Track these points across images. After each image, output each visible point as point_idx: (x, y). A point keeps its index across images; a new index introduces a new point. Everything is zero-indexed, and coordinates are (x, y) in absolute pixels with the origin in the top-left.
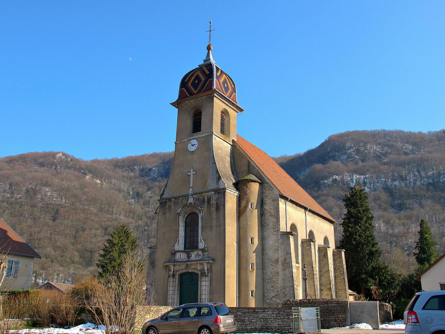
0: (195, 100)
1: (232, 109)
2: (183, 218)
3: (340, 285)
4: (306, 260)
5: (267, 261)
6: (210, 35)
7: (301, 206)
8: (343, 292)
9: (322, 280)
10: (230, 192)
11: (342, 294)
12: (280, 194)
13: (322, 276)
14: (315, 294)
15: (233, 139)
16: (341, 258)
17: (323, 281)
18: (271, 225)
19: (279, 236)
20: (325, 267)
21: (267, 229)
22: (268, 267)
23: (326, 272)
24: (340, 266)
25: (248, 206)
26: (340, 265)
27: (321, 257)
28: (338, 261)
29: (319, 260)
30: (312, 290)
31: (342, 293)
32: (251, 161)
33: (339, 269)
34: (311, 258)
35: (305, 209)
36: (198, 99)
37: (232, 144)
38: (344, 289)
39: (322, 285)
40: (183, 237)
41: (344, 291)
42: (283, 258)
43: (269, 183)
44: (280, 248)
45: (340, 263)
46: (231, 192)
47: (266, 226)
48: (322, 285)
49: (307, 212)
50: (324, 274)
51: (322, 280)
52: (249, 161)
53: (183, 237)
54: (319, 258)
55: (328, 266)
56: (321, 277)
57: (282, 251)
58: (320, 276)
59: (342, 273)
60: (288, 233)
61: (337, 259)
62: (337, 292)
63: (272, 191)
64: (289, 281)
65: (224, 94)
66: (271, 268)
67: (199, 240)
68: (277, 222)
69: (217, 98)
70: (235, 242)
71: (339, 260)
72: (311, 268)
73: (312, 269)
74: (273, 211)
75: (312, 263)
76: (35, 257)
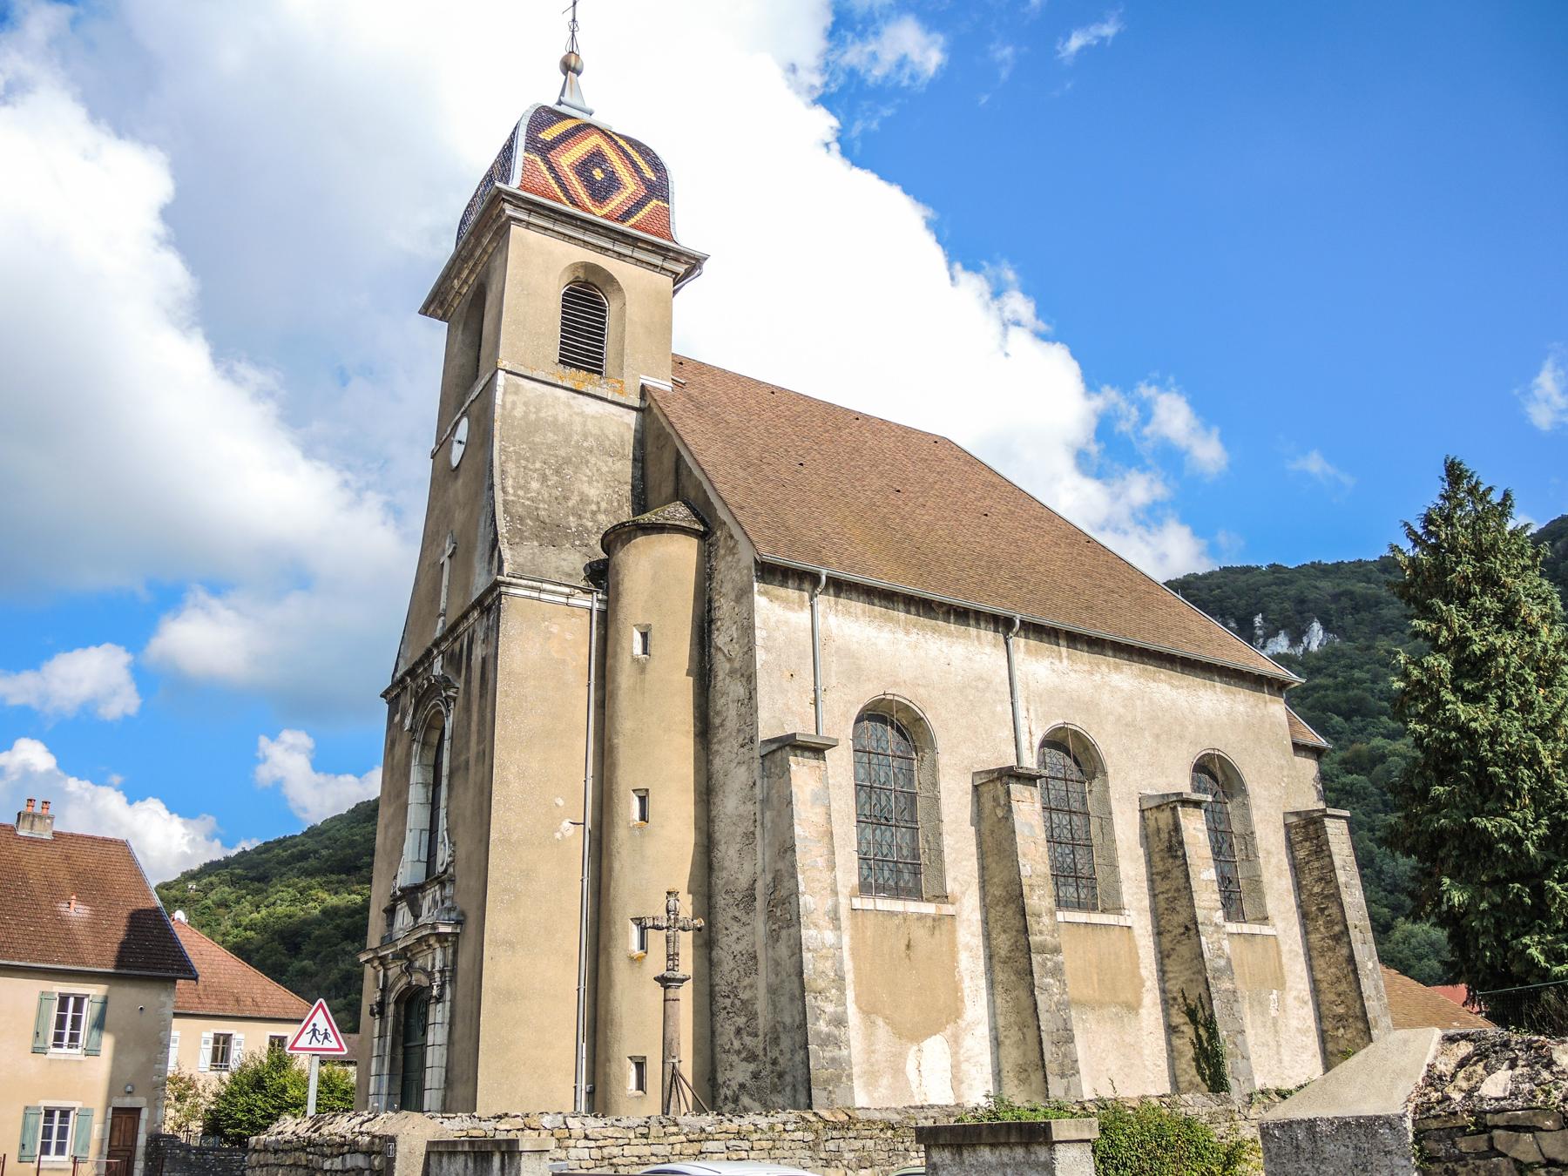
0: (471, 264)
1: (639, 262)
2: (422, 749)
3: (1339, 995)
4: (996, 880)
5: (723, 902)
6: (574, 20)
7: (962, 615)
8: (1356, 1028)
9: (1170, 979)
10: (535, 594)
11: (1349, 1041)
12: (758, 558)
13: (1168, 956)
14: (1043, 1060)
15: (650, 382)
16: (1327, 853)
17: (1173, 982)
18: (732, 723)
19: (757, 764)
20: (1178, 908)
21: (720, 742)
22: (727, 929)
23: (1184, 934)
24: (1326, 897)
25: (625, 644)
26: (1323, 889)
27: (1156, 858)
28: (1316, 873)
29: (1152, 874)
30: (1028, 1038)
31: (1349, 1036)
32: (683, 452)
33: (1322, 910)
34: (1015, 863)
35: (1002, 624)
36: (477, 254)
37: (637, 404)
38: (1359, 1013)
39: (1171, 1002)
40: (421, 830)
41: (1361, 1025)
42: (769, 878)
43: (725, 523)
44: (758, 824)
45: (1322, 879)
46: (543, 596)
47: (718, 728)
48: (1172, 1006)
49: (1019, 643)
50: (1178, 942)
51: (1170, 979)
52: (678, 452)
53: (421, 830)
54: (1151, 867)
55: (1191, 899)
56: (1166, 961)
57: (767, 841)
58: (1162, 958)
59: (1337, 929)
60: (774, 747)
61: (1307, 863)
62: (1326, 1031)
63: (734, 554)
64: (792, 999)
65: (590, 212)
66: (735, 936)
67: (440, 840)
68: (750, 698)
69: (528, 225)
70: (566, 824)
71: (1316, 864)
72: (1019, 916)
73: (1022, 923)
74: (736, 646)
75: (1017, 887)
76: (181, 978)
